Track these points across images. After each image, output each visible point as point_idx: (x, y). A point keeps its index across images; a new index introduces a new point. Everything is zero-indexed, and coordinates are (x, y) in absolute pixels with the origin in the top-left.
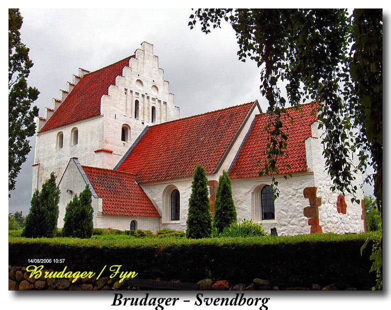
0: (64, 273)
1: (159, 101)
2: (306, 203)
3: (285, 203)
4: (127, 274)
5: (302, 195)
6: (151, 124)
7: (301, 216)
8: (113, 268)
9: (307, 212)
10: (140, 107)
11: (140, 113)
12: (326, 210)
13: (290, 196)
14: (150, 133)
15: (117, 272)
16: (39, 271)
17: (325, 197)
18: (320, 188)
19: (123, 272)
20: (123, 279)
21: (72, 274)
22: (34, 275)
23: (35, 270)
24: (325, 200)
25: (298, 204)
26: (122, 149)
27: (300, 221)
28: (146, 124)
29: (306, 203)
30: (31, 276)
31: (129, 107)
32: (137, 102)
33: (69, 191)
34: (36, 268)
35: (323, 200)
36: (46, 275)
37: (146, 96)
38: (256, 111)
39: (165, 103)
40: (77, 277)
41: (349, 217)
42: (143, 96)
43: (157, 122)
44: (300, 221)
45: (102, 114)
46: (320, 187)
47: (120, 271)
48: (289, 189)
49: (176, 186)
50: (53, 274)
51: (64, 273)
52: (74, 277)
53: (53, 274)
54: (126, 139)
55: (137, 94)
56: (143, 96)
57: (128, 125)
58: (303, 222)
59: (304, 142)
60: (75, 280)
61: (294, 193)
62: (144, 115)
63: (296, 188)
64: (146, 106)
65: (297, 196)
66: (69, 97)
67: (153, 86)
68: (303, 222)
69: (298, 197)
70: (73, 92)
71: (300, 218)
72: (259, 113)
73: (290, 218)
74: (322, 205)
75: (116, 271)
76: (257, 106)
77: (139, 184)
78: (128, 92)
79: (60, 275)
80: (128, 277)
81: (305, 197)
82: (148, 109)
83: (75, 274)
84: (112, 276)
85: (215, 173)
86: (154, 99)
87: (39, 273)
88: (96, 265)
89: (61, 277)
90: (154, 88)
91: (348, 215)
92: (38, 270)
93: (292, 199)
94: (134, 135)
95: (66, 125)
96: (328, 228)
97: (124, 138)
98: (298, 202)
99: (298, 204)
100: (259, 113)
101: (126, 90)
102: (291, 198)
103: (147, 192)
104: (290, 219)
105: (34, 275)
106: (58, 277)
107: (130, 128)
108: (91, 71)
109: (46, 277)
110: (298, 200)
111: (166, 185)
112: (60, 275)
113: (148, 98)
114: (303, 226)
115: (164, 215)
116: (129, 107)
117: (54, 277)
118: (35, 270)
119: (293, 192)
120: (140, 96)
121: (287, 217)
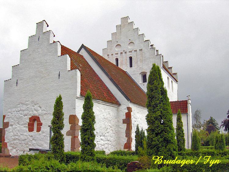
0: (176, 161)
2: (127, 111)
4: (215, 161)
8: (205, 158)
10: (119, 62)
15: (208, 160)
16: (161, 159)
19: (212, 160)
20: (212, 164)
21: (186, 162)
22: (158, 162)
23: (158, 159)
29: (127, 111)
30: (155, 163)
34: (159, 158)
35: (10, 123)
36: (165, 162)
40: (184, 163)
41: (44, 134)
46: (8, 114)
47: (210, 160)
50: (169, 162)
51: (176, 161)
52: (182, 163)
53: (169, 162)
60: (183, 165)
74: (10, 127)
75: (207, 160)
79: (178, 162)
80: (215, 163)
83: (182, 161)
84: (205, 163)
87: (160, 161)
88: (18, 171)
89: (174, 163)
90: (131, 44)
91: (43, 132)
92: (159, 159)
101: (108, 55)
105: (158, 162)
106: (172, 163)
109: (164, 163)
112: (178, 162)
117: (170, 163)
118: (158, 159)
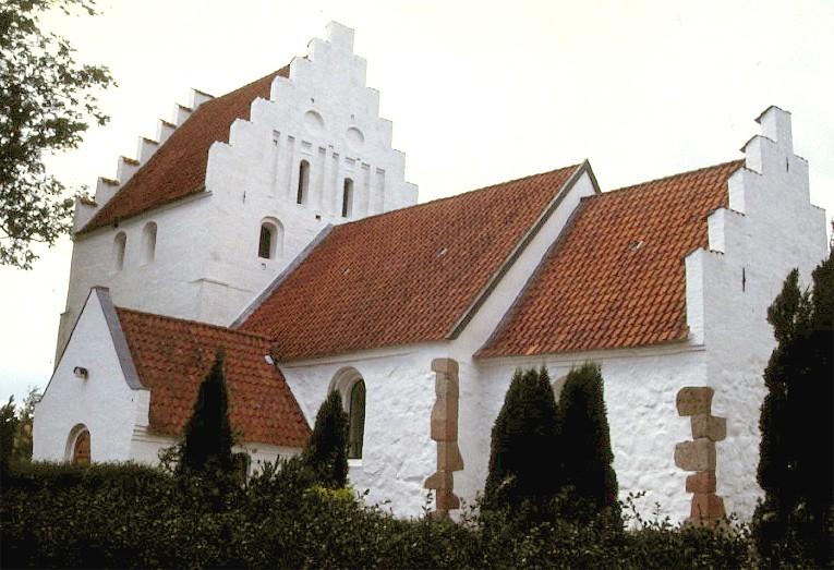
1: (366, 166)
3: (628, 427)
5: (673, 407)
6: (340, 221)
7: (666, 467)
9: (683, 455)
11: (311, 191)
12: (740, 454)
13: (642, 409)
14: (334, 242)
17: (738, 416)
18: (724, 392)
24: (737, 425)
25: (662, 431)
26: (261, 277)
27: (664, 479)
28: (326, 221)
31: (281, 176)
32: (304, 166)
33: (78, 370)
35: (732, 425)
37: (328, 150)
38: (583, 188)
39: (381, 172)
42: (322, 150)
43: (356, 215)
44: (664, 479)
45: (207, 190)
46: (725, 387)
48: (642, 391)
49: (361, 372)
54: (271, 254)
55: (307, 144)
56: (322, 150)
57: (275, 219)
58: (673, 484)
59: (682, 262)
61: (653, 402)
62: (321, 197)
63: (658, 388)
64: (329, 176)
65: (659, 408)
66: (160, 152)
67: (310, 112)
68: (673, 484)
69: (662, 412)
70: (171, 143)
71: (665, 472)
72: (594, 193)
73: (639, 469)
74: (730, 439)
76: (586, 174)
77: (276, 362)
78: (283, 139)
81: (682, 413)
82: (334, 182)
85: (449, 339)
86: (350, 160)
90: (354, 134)
93: (646, 417)
94: (292, 248)
95: (136, 215)
96: (744, 504)
97: (265, 249)
98: (661, 425)
99: (662, 431)
100: (590, 192)
101: (276, 133)
102: (643, 414)
103: (349, 411)
104: (637, 474)
107: (282, 227)
108: (218, 94)
110: (660, 421)
111: (337, 368)
113: (335, 155)
114: (670, 495)
115: (404, 483)
116: (281, 176)
119: (650, 398)
120: (315, 151)
121: (630, 465)
